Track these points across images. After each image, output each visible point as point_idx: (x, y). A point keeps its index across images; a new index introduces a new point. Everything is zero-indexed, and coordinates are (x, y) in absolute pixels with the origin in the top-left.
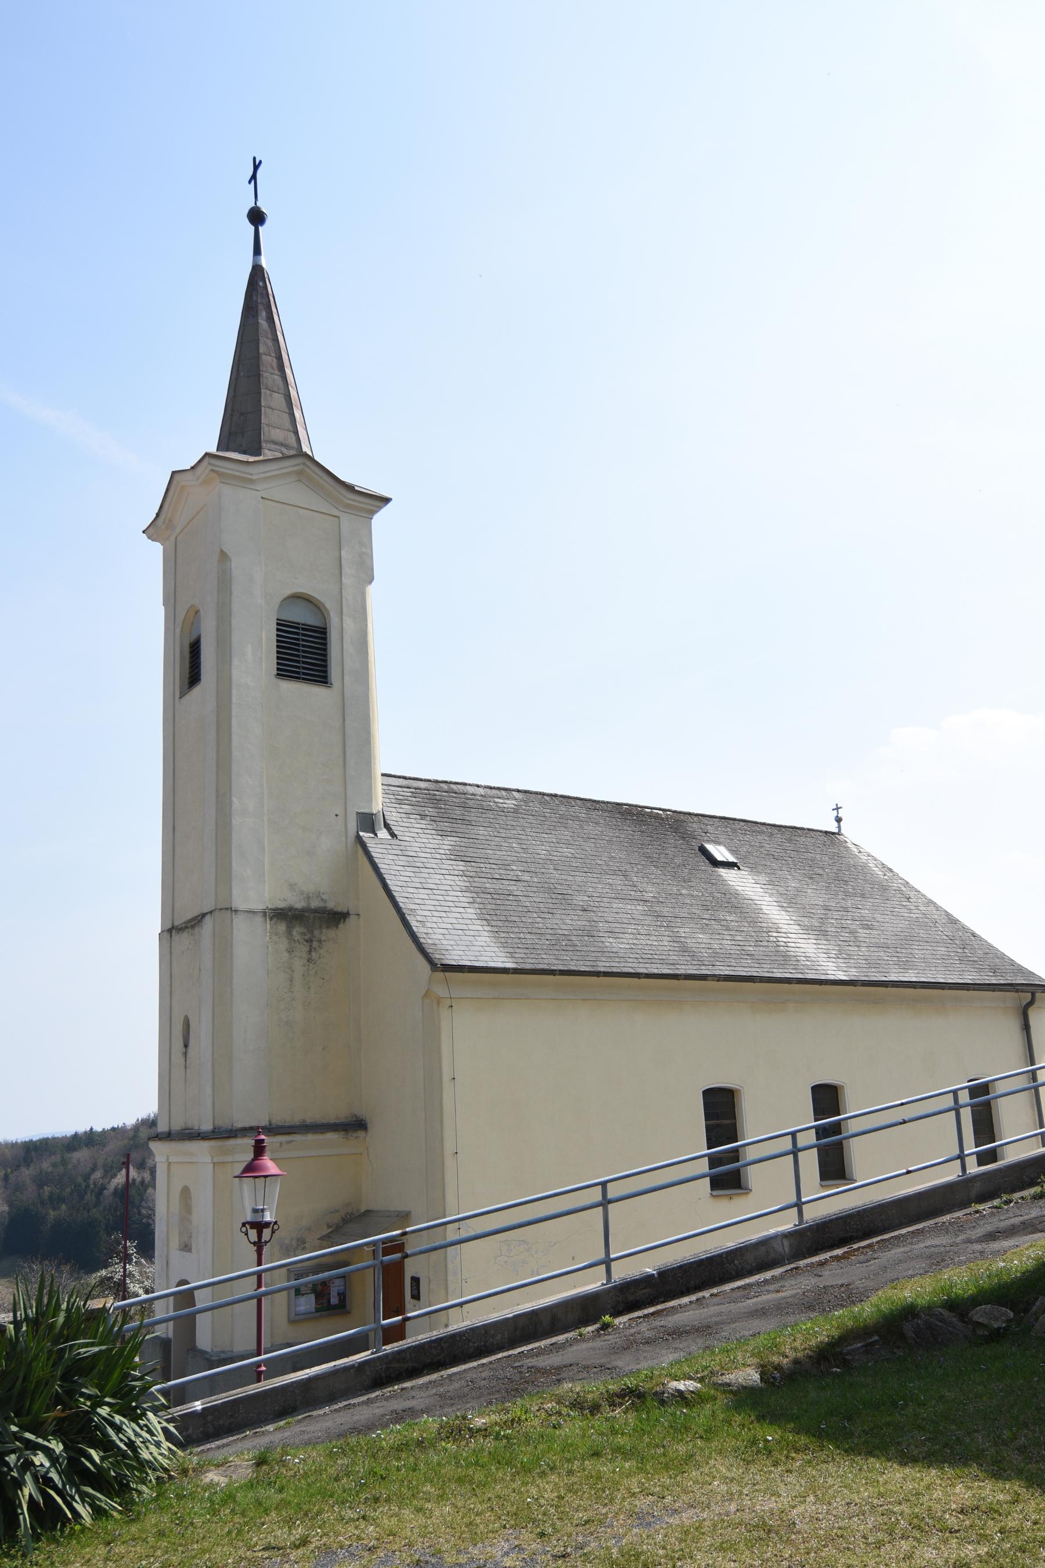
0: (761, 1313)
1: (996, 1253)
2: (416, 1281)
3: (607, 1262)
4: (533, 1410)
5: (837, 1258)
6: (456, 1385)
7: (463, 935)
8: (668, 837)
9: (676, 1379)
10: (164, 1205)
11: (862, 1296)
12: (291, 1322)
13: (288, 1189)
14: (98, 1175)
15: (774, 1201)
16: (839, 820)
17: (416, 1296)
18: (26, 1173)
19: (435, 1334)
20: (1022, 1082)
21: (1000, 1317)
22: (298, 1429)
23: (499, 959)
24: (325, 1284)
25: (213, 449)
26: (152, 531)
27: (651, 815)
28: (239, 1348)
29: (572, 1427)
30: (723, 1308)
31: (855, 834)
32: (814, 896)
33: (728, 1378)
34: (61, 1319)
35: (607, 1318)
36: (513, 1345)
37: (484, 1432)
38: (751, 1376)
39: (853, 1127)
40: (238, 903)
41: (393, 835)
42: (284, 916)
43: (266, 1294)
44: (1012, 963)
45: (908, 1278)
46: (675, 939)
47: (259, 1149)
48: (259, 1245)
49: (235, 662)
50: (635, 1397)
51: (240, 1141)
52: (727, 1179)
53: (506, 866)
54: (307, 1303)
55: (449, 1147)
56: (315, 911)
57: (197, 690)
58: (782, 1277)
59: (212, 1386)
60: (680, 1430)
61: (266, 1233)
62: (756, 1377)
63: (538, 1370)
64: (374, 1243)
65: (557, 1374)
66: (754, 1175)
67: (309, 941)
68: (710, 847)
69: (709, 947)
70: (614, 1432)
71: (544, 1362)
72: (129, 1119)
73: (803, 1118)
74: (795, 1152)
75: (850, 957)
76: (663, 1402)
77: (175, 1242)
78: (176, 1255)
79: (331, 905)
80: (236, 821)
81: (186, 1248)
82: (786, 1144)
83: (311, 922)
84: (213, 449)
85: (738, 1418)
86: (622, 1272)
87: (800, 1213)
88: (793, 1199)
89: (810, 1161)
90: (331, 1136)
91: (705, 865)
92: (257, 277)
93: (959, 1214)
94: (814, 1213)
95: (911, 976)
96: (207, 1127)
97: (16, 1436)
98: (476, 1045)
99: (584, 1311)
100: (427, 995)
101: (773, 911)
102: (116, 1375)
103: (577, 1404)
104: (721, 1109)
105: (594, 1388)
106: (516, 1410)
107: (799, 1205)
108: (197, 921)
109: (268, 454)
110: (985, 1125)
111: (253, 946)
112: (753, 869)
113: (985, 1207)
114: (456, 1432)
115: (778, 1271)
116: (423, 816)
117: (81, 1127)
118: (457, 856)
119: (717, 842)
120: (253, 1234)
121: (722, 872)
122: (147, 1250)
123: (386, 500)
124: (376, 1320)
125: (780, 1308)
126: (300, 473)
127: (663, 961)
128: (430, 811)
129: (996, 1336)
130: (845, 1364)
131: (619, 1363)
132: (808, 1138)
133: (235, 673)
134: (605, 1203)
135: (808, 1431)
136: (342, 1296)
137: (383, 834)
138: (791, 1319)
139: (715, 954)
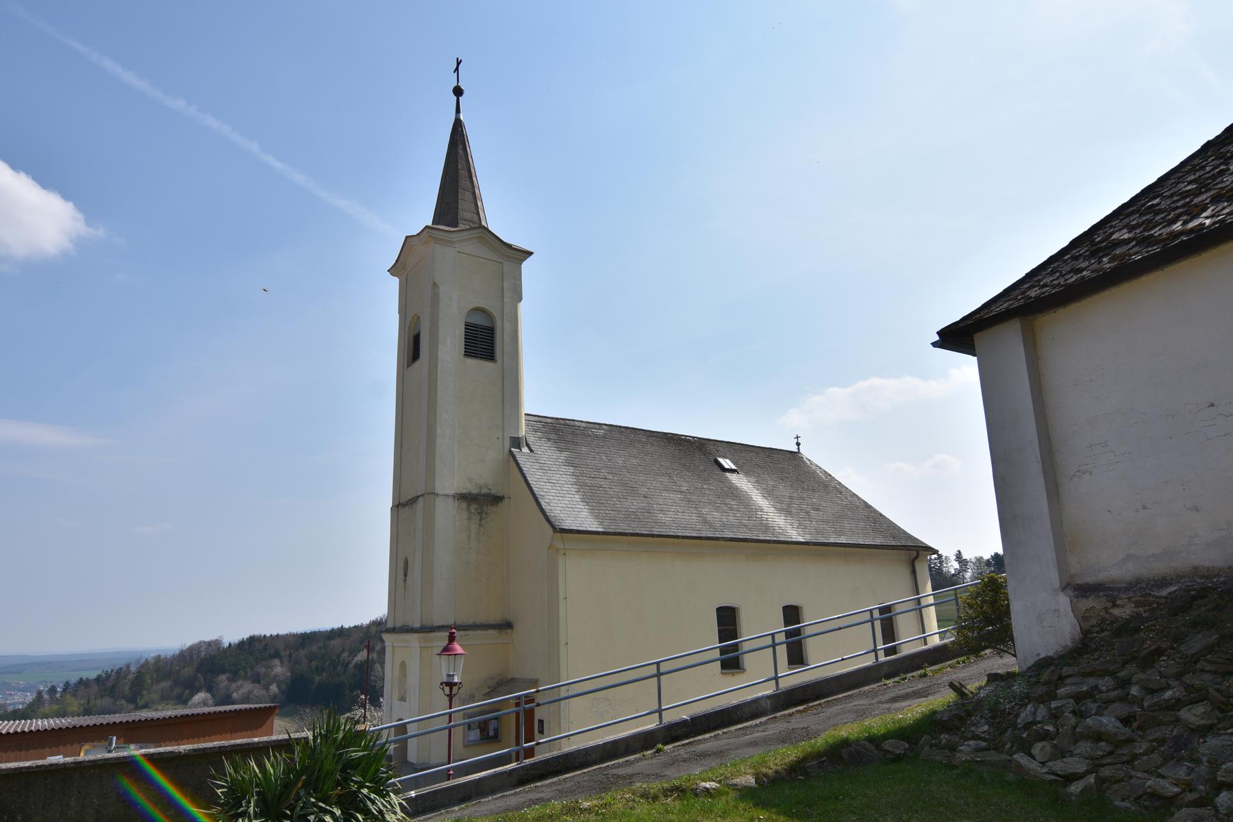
0: (754, 744)
1: (897, 710)
2: (541, 722)
3: (660, 711)
4: (618, 799)
5: (799, 712)
6: (569, 785)
7: (570, 508)
8: (696, 455)
9: (704, 780)
10: (390, 672)
11: (816, 734)
12: (465, 746)
13: (467, 663)
14: (345, 655)
15: (760, 677)
16: (798, 444)
17: (541, 732)
18: (302, 652)
19: (556, 753)
20: (911, 606)
21: (900, 747)
22: (473, 809)
23: (594, 526)
24: (486, 722)
25: (430, 224)
26: (393, 271)
27: (685, 440)
28: (433, 761)
29: (642, 808)
30: (731, 741)
31: (809, 453)
32: (784, 490)
33: (737, 781)
34: (341, 735)
35: (660, 746)
36: (603, 760)
37: (589, 810)
38: (749, 780)
39: (808, 631)
40: (439, 490)
41: (531, 450)
42: (466, 498)
43: (454, 726)
44: (905, 533)
45: (844, 723)
46: (700, 515)
47: (452, 638)
48: (451, 697)
49: (440, 347)
50: (679, 791)
51: (439, 634)
52: (731, 663)
53: (598, 470)
54: (475, 735)
55: (562, 640)
56: (484, 495)
57: (417, 364)
58: (766, 722)
59: (415, 783)
60: (707, 811)
61: (455, 689)
62: (753, 781)
63: (618, 776)
64: (519, 697)
65: (630, 778)
66: (748, 661)
67: (480, 513)
68: (721, 460)
69: (721, 520)
70: (667, 812)
71: (621, 771)
72: (364, 619)
73: (779, 626)
74: (774, 645)
75: (805, 527)
76: (696, 795)
77: (396, 696)
78: (396, 703)
79: (493, 492)
80: (439, 441)
81: (403, 699)
82: (769, 641)
83: (481, 501)
84: (430, 224)
85: (742, 805)
86: (669, 718)
87: (777, 684)
88: (773, 675)
89: (782, 651)
90: (491, 632)
91: (717, 471)
92: (458, 127)
93: (874, 686)
94: (785, 684)
95: (843, 540)
96: (417, 625)
97: (314, 805)
98: (578, 576)
99: (645, 741)
100: (550, 547)
101: (758, 498)
102: (372, 770)
103: (645, 795)
104: (728, 620)
105: (655, 786)
106: (608, 798)
107: (776, 678)
108: (414, 500)
109: (462, 227)
110: (889, 632)
111: (447, 518)
112: (747, 474)
113: (890, 682)
114: (572, 810)
115: (764, 719)
116: (549, 440)
117: (336, 625)
118: (569, 463)
119: (724, 457)
120: (447, 689)
121: (728, 475)
122: (376, 703)
123: (531, 253)
124: (518, 743)
125: (766, 741)
126: (481, 238)
127: (693, 529)
128: (553, 436)
129: (898, 759)
130: (806, 773)
131: (668, 773)
132: (781, 638)
133: (440, 354)
134: (659, 675)
135: (785, 814)
136: (496, 731)
137: (525, 450)
138: (773, 748)
139: (724, 525)
